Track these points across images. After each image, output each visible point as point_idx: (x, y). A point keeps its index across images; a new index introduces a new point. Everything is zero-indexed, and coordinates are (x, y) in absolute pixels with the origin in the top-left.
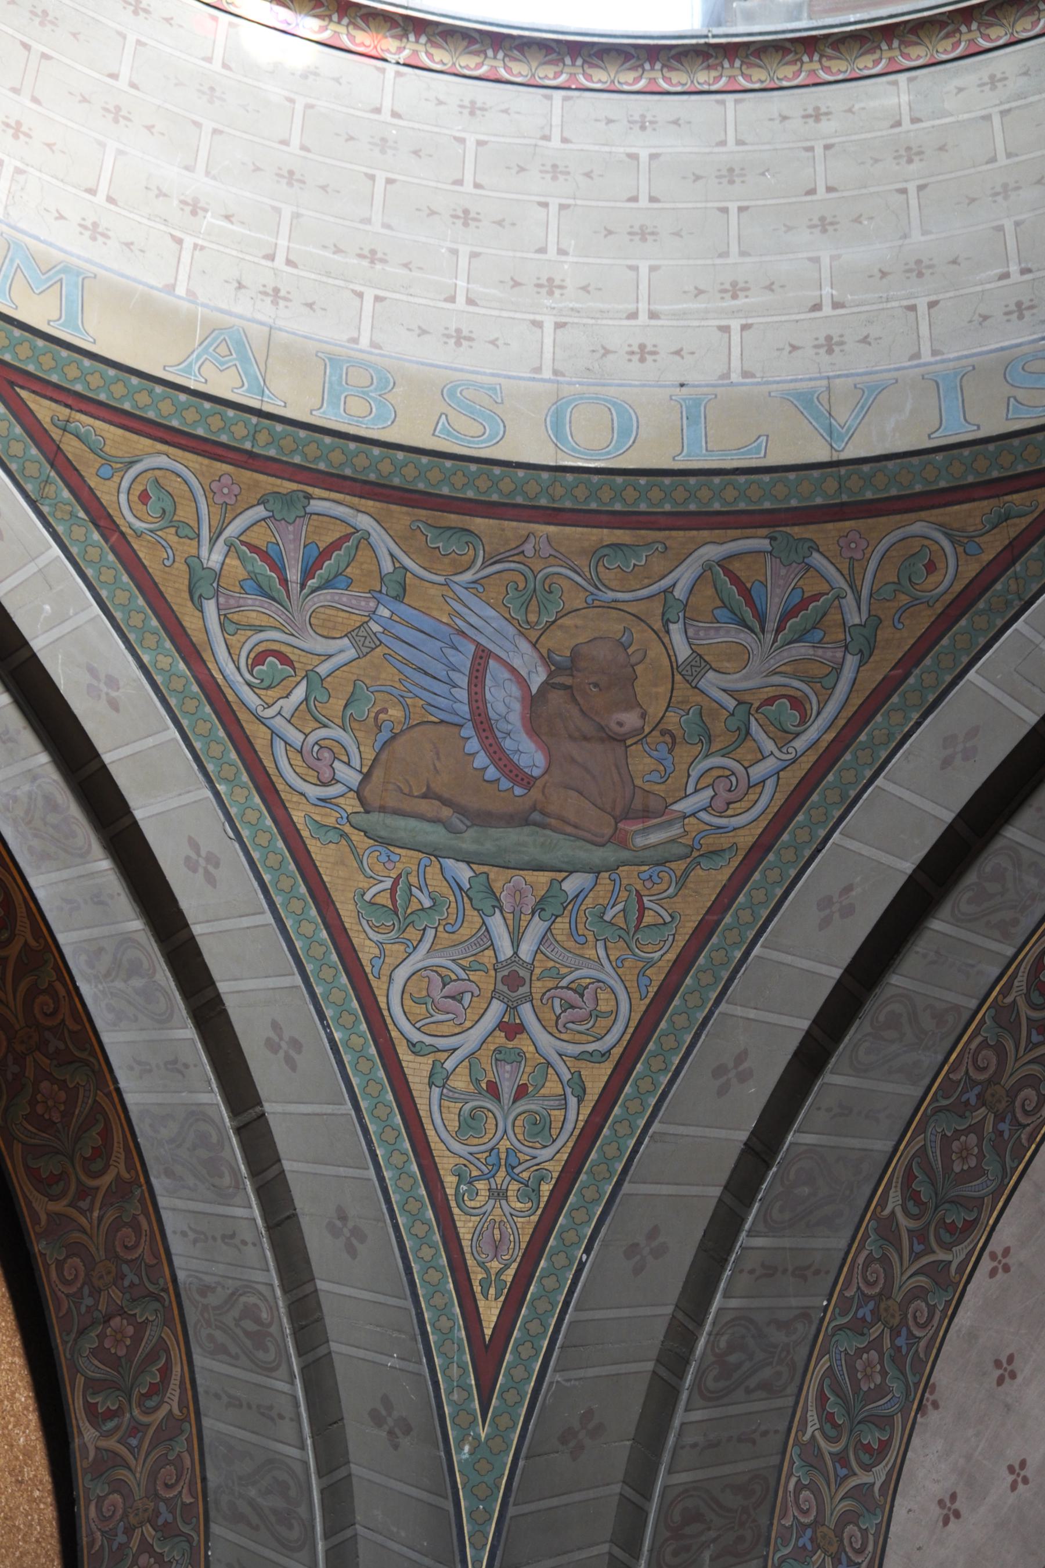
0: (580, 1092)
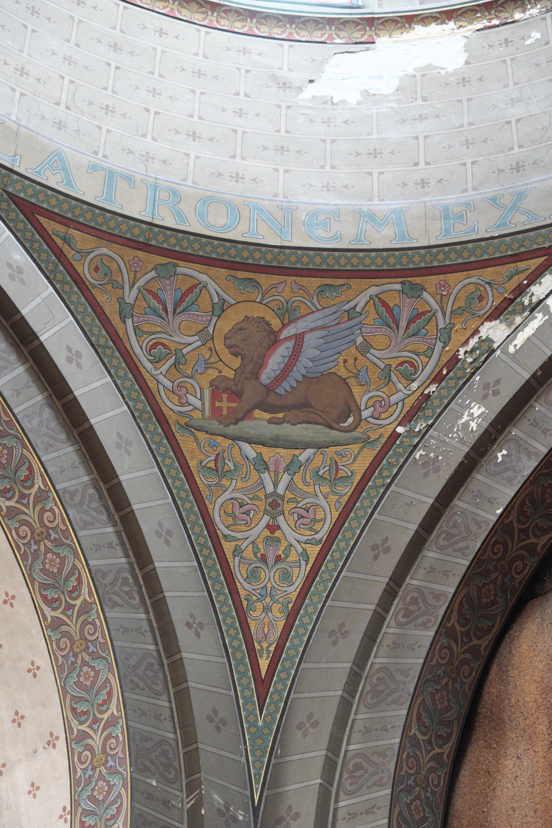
0: (306, 559)
